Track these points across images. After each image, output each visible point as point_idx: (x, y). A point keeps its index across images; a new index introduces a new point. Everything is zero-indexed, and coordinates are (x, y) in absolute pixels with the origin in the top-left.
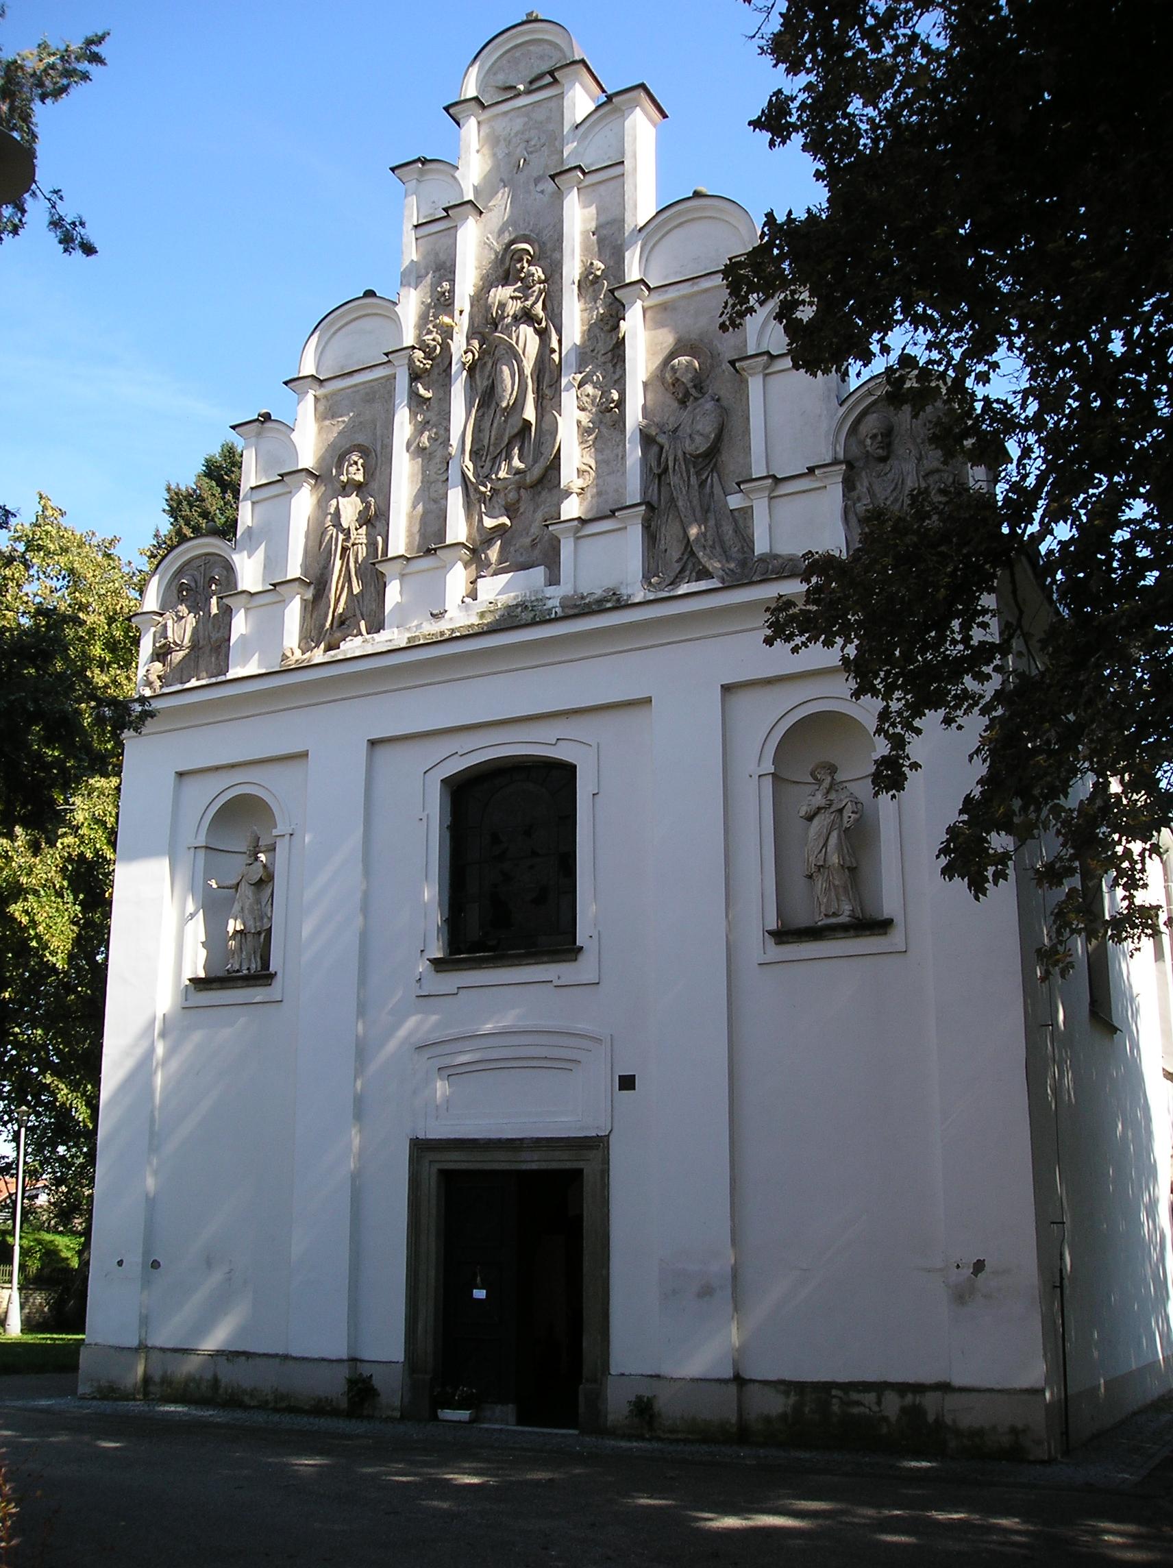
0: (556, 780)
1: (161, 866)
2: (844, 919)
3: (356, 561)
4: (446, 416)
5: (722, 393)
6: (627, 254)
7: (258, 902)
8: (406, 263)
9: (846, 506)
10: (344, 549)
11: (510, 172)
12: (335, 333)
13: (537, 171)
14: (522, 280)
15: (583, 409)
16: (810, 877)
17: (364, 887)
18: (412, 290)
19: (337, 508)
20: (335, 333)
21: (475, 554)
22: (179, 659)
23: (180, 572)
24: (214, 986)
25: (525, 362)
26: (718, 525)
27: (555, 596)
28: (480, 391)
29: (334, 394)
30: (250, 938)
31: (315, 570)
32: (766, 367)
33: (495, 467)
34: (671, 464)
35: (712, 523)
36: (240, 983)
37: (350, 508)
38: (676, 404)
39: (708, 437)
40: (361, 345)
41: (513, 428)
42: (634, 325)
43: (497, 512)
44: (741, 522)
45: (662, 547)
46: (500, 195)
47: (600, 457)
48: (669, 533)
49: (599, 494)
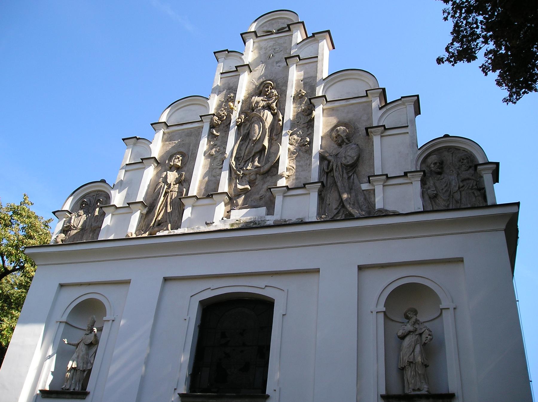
0: (263, 307)
1: (40, 328)
2: (424, 392)
3: (171, 198)
4: (225, 143)
5: (359, 143)
6: (317, 88)
7: (87, 354)
8: (215, 85)
9: (422, 191)
10: (166, 193)
11: (265, 58)
12: (177, 110)
13: (280, 57)
14: (267, 95)
15: (291, 144)
16: (402, 369)
17: (148, 351)
18: (216, 95)
19: (166, 175)
20: (177, 110)
21: (231, 202)
22: (74, 233)
23: (84, 197)
24: (53, 396)
25: (266, 124)
26: (356, 196)
27: (270, 220)
28: (242, 134)
29: (172, 132)
30: (78, 373)
31: (150, 200)
32: (382, 133)
33: (246, 163)
34: (334, 167)
35: (353, 194)
36: (68, 396)
37: (172, 176)
38: (336, 146)
39: (353, 158)
40: (191, 114)
41: (258, 148)
42: (318, 113)
43: (244, 183)
44: (367, 196)
45: (328, 203)
46: (260, 66)
47: (298, 164)
48: (332, 198)
49: (297, 179)
